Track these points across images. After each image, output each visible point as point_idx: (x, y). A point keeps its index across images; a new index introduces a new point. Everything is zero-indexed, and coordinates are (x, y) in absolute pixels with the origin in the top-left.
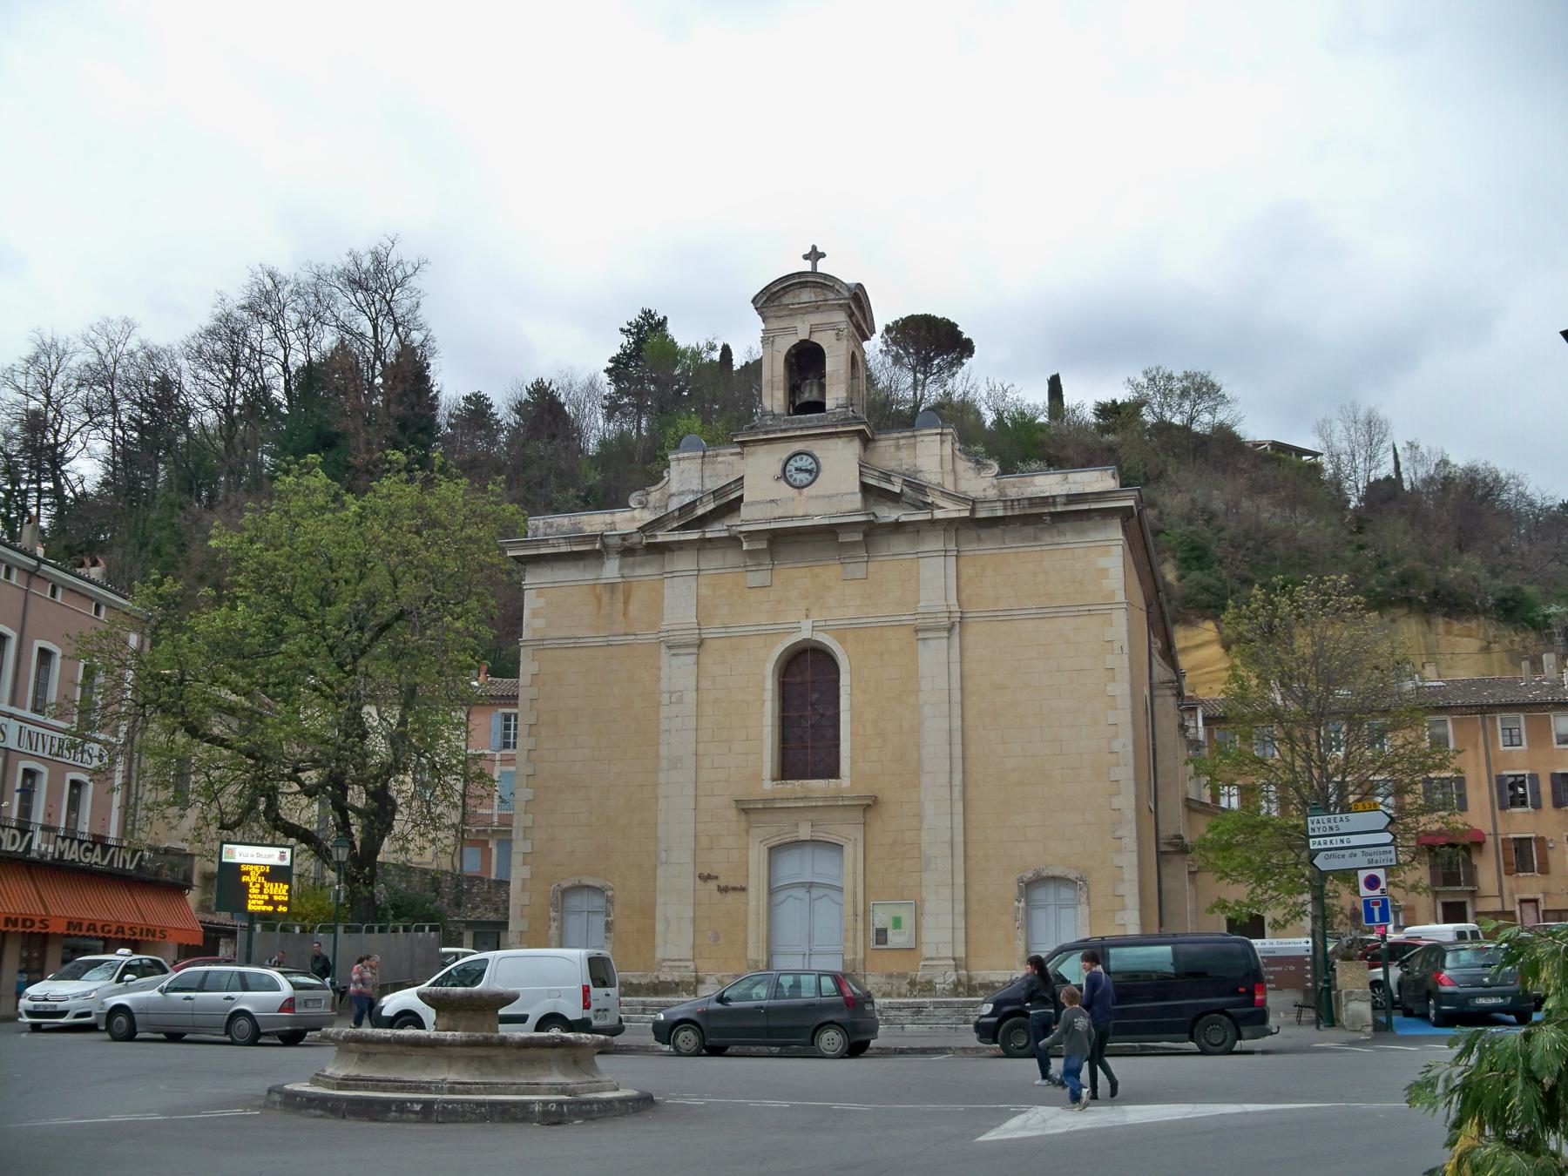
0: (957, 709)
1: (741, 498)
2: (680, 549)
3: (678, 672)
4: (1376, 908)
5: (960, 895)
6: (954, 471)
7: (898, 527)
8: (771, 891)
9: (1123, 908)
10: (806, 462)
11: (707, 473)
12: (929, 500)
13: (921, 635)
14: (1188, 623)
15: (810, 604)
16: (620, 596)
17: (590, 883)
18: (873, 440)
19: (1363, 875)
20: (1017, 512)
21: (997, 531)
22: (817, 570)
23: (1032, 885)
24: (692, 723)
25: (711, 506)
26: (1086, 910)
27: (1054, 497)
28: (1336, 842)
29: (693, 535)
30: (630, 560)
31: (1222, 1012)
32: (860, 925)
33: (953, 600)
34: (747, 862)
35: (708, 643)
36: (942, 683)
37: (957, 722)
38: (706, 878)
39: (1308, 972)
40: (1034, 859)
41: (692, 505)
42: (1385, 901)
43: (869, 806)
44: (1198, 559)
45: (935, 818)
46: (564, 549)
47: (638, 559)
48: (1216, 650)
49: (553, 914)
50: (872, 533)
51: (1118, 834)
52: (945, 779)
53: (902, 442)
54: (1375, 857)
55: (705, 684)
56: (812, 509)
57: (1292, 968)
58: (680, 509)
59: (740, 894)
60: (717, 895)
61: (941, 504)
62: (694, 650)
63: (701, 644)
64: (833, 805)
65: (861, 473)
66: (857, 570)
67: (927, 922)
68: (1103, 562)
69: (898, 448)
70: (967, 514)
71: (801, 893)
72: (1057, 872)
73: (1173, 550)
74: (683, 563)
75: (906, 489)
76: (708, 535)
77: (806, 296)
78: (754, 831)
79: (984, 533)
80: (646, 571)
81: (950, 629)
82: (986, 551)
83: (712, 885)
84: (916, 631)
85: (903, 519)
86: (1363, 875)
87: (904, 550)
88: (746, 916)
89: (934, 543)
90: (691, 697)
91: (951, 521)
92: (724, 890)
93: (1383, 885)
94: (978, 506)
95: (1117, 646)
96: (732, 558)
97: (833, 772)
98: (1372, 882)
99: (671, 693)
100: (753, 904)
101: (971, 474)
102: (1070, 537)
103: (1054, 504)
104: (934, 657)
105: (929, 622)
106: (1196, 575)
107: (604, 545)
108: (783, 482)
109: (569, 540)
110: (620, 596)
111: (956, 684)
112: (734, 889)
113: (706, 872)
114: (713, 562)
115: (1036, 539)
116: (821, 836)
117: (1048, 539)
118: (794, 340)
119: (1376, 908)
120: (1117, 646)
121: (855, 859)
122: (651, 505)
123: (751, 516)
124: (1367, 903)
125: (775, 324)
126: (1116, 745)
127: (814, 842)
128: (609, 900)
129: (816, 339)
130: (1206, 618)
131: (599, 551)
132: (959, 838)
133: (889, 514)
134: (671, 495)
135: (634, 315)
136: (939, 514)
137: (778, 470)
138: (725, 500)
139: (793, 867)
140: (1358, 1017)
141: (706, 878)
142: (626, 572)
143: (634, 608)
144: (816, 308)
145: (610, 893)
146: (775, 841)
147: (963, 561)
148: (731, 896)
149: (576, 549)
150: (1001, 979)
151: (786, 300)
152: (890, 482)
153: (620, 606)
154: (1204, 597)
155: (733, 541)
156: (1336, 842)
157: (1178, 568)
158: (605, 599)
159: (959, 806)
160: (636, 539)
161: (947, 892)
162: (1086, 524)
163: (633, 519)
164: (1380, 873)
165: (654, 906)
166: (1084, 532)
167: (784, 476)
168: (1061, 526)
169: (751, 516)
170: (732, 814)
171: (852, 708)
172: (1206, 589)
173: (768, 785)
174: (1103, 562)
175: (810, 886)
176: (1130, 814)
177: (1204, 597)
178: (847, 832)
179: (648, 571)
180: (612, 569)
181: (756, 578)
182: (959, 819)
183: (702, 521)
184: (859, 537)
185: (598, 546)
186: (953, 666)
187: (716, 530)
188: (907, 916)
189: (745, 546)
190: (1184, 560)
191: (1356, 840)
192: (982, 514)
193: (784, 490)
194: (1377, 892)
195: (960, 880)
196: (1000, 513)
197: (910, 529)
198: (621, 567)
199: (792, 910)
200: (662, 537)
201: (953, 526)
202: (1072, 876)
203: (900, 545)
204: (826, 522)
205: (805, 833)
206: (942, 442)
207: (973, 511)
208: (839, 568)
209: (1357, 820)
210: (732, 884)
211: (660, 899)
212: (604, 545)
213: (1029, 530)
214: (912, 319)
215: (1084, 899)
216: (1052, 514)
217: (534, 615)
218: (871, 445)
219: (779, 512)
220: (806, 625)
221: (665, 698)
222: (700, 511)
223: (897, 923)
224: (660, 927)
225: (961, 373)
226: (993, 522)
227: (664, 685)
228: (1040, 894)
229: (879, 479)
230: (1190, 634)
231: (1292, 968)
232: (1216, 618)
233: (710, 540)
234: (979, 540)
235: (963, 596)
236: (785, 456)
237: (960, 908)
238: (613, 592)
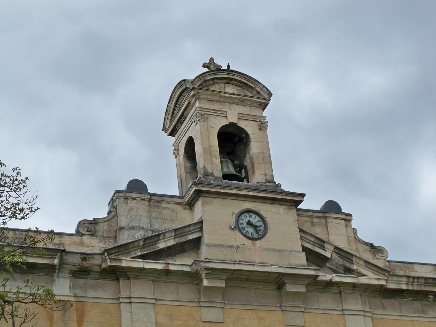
2: (137, 277)
10: (255, 220)
11: (154, 215)
12: (355, 267)
16: (73, 314)
21: (395, 302)
22: (262, 314)
25: (171, 242)
29: (158, 266)
30: (81, 281)
41: (157, 237)
47: (90, 282)
53: (315, 220)
56: (269, 258)
58: (145, 240)
61: (363, 271)
74: (140, 290)
75: (335, 256)
76: (171, 268)
77: (230, 89)
79: (386, 302)
80: (100, 294)
87: (331, 307)
89: (354, 304)
96: (186, 292)
108: (238, 232)
114: (168, 293)
115: (423, 312)
118: (225, 122)
122: (99, 234)
129: (242, 124)
131: (53, 267)
134: (121, 229)
136: (363, 280)
137: (232, 221)
138: (183, 239)
142: (79, 292)
151: (216, 88)
152: (323, 248)
155: (193, 277)
160: (97, 261)
163: (82, 244)
179: (100, 294)
180: (62, 288)
185: (56, 262)
187: (181, 263)
189: (206, 283)
193: (238, 238)
196: (404, 287)
197: (334, 289)
198: (72, 287)
200: (126, 262)
203: (326, 301)
208: (280, 314)
212: (62, 263)
213: (417, 304)
219: (238, 257)
222: (162, 245)
229: (314, 244)
233: (24, 247)
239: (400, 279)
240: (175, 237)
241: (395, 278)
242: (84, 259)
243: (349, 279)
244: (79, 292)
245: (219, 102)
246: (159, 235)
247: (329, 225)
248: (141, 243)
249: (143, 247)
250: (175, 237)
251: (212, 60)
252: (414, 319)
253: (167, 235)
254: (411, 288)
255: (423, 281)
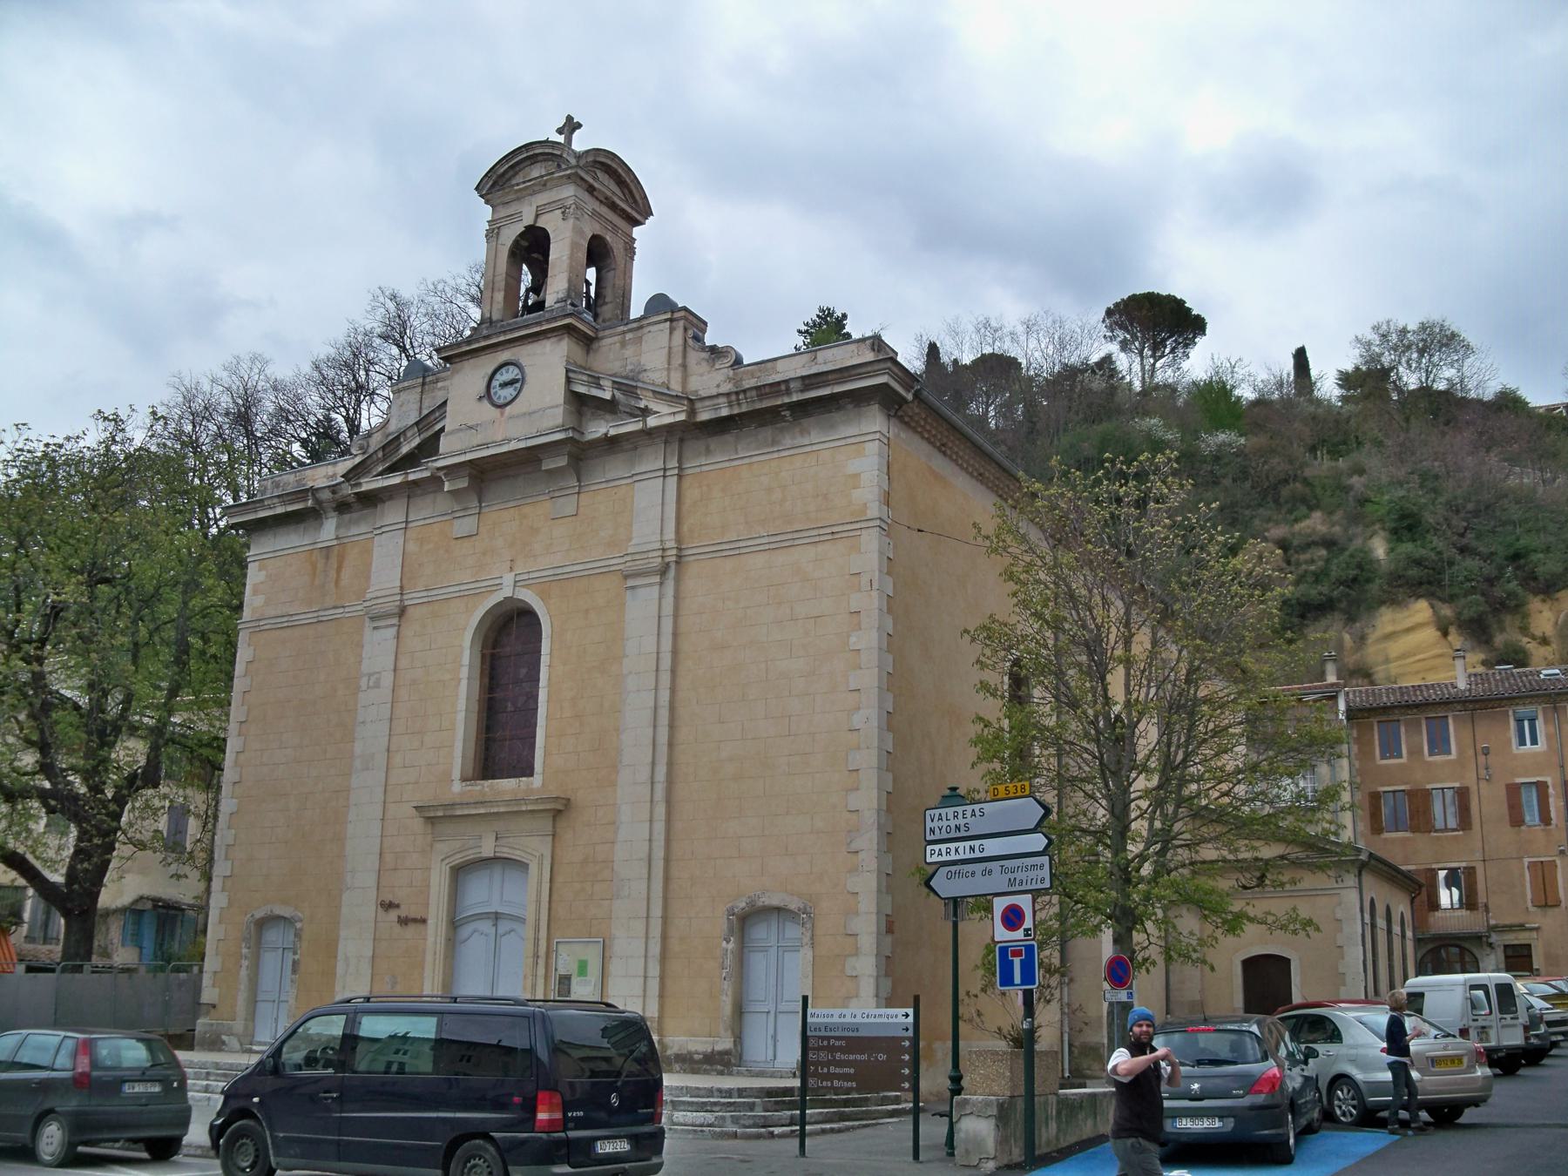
0: (665, 678)
1: (443, 429)
2: (391, 498)
3: (378, 646)
4: (1017, 961)
5: (656, 931)
6: (684, 366)
7: (611, 444)
8: (454, 924)
9: (856, 953)
10: (510, 374)
13: (630, 583)
14: (1394, 602)
15: (510, 550)
16: (334, 562)
17: (282, 913)
18: (597, 339)
19: (1000, 905)
20: (744, 409)
22: (526, 510)
23: (746, 920)
24: (385, 711)
25: (417, 441)
26: (806, 953)
27: (786, 382)
28: (963, 850)
29: (395, 479)
30: (347, 517)
31: (486, 1136)
32: (541, 971)
33: (670, 534)
34: (428, 886)
35: (411, 612)
36: (650, 645)
37: (665, 696)
38: (389, 906)
39: (904, 1064)
40: (749, 881)
41: (395, 442)
42: (1030, 949)
43: (559, 811)
44: (1410, 528)
45: (629, 826)
46: (280, 510)
47: (355, 515)
48: (1431, 634)
49: (245, 951)
50: (580, 455)
51: (854, 847)
52: (644, 774)
53: (629, 336)
54: (1020, 875)
55: (403, 663)
57: (882, 1057)
58: (384, 448)
59: (421, 927)
60: (397, 929)
62: (395, 621)
63: (402, 612)
64: (515, 813)
65: (569, 381)
66: (568, 505)
67: (615, 967)
68: (854, 466)
69: (623, 344)
70: (682, 417)
71: (486, 926)
72: (775, 901)
73: (1381, 520)
74: (392, 514)
75: (618, 394)
76: (412, 477)
77: (536, 171)
78: (438, 846)
79: (714, 442)
81: (663, 571)
82: (714, 464)
83: (393, 915)
84: (626, 577)
85: (612, 432)
86: (1000, 905)
87: (621, 474)
88: (424, 951)
89: (652, 461)
90: (387, 680)
91: (669, 428)
92: (404, 921)
93: (1028, 923)
94: (698, 405)
95: (865, 580)
97: (529, 772)
98: (1013, 918)
99: (370, 675)
100: (431, 939)
101: (705, 367)
102: (815, 436)
103: (788, 392)
104: (644, 607)
105: (640, 565)
106: (1407, 547)
107: (317, 501)
109: (285, 498)
110: (334, 562)
111: (667, 644)
112: (415, 920)
113: (388, 898)
114: (426, 510)
115: (774, 443)
116: (505, 852)
117: (788, 442)
118: (519, 228)
119: (1017, 961)
120: (865, 580)
121: (540, 883)
123: (452, 449)
124: (1004, 951)
125: (503, 212)
126: (857, 720)
127: (495, 859)
128: (298, 935)
130: (1419, 597)
132: (659, 854)
133: (598, 429)
135: (812, 315)
136: (652, 422)
139: (481, 893)
140: (977, 1142)
141: (389, 906)
143: (346, 575)
144: (543, 185)
145: (298, 925)
146: (458, 859)
147: (686, 483)
148: (411, 930)
149: (290, 508)
150: (701, 1048)
152: (600, 387)
153: (333, 574)
154: (1414, 572)
155: (434, 482)
156: (963, 850)
157: (1389, 541)
158: (320, 566)
159: (660, 810)
161: (639, 926)
162: (836, 416)
164: (1024, 902)
165: (337, 941)
166: (832, 427)
167: (488, 394)
168: (805, 422)
169: (452, 449)
170: (417, 824)
171: (549, 685)
172: (1418, 562)
173: (457, 787)
174: (854, 466)
175: (496, 917)
176: (870, 817)
177: (1414, 572)
178: (532, 846)
180: (329, 529)
181: (465, 525)
182: (660, 827)
183: (411, 460)
184: (562, 462)
185: (310, 503)
186: (664, 620)
188: (593, 956)
190: (1394, 531)
191: (993, 847)
192: (704, 416)
194: (1019, 934)
195: (657, 911)
196: (725, 412)
198: (338, 527)
199: (476, 944)
200: (368, 484)
201: (668, 432)
202: (793, 906)
204: (522, 445)
205: (487, 850)
206: (672, 330)
207: (692, 412)
208: (548, 504)
209: (995, 813)
210: (412, 915)
211: (343, 933)
212: (317, 501)
213: (767, 433)
214: (1133, 298)
215: (806, 940)
216: (792, 407)
217: (255, 592)
218: (595, 346)
220: (508, 579)
221: (364, 682)
222: (405, 450)
223: (583, 968)
224: (340, 970)
225: (1194, 352)
226: (720, 426)
227: (365, 668)
228: (762, 933)
230: (1399, 616)
231: (882, 1057)
232: (1430, 596)
233: (414, 482)
234: (708, 452)
235: (685, 528)
236: (490, 371)
237: (655, 949)
238: (327, 558)
239: (716, 401)
240: (420, 432)
241: (707, 403)
242: (334, 492)
243: (632, 426)
244: (342, 533)
245: (518, 199)
246: (398, 438)
247: (173, 390)
248: (380, 454)
249: (385, 458)
250: (420, 432)
251: (579, 126)
252: (755, 459)
253: (409, 434)
254: (736, 411)
255: (754, 393)
